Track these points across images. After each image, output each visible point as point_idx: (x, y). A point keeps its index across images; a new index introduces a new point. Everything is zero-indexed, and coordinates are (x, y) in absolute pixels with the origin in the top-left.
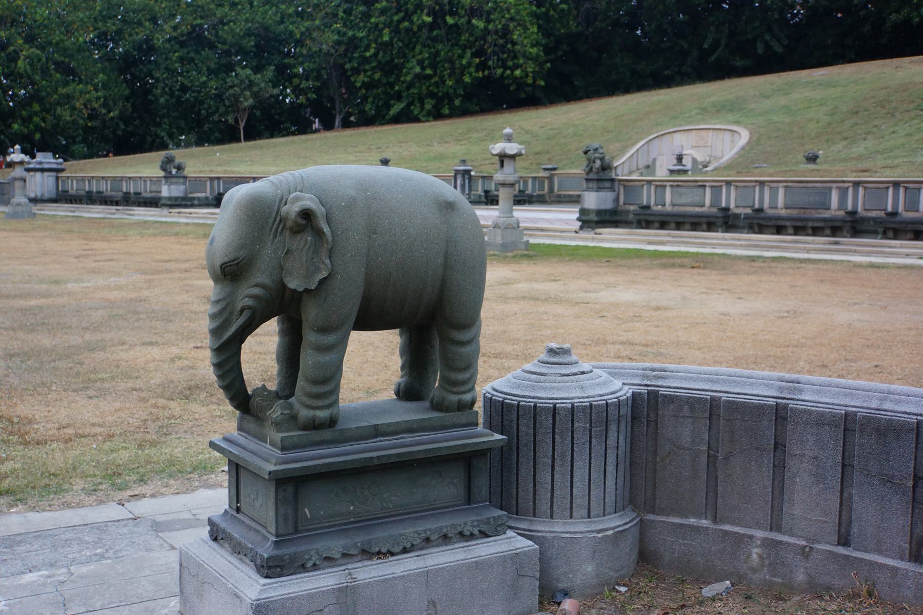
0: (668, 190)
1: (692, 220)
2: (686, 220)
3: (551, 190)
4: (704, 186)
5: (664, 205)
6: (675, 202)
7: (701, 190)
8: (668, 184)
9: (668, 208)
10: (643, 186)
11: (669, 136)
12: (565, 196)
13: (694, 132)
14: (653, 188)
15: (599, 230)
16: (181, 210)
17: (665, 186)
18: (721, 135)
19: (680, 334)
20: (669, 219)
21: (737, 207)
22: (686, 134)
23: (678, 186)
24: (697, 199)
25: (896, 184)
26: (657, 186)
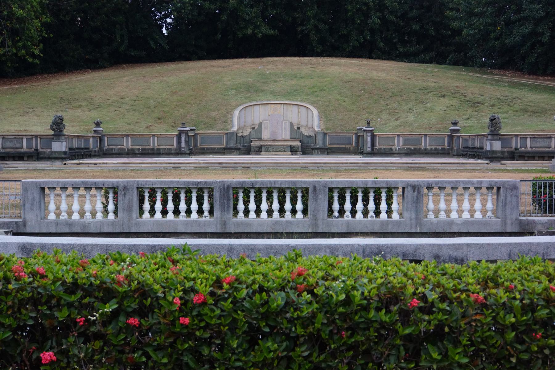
0: (528, 140)
1: (539, 155)
2: (546, 155)
3: (195, 145)
4: (551, 137)
5: (525, 148)
6: (533, 146)
7: (549, 140)
8: (529, 136)
9: (529, 149)
10: (512, 138)
11: (250, 107)
12: (208, 149)
13: (269, 105)
14: (519, 138)
15: (503, 162)
16: (81, 161)
17: (527, 138)
18: (290, 108)
19: (389, 268)
20: (535, 155)
21: (521, 148)
22: (263, 107)
23: (534, 137)
24: (546, 144)
25: (399, 135)
26: (521, 138)
